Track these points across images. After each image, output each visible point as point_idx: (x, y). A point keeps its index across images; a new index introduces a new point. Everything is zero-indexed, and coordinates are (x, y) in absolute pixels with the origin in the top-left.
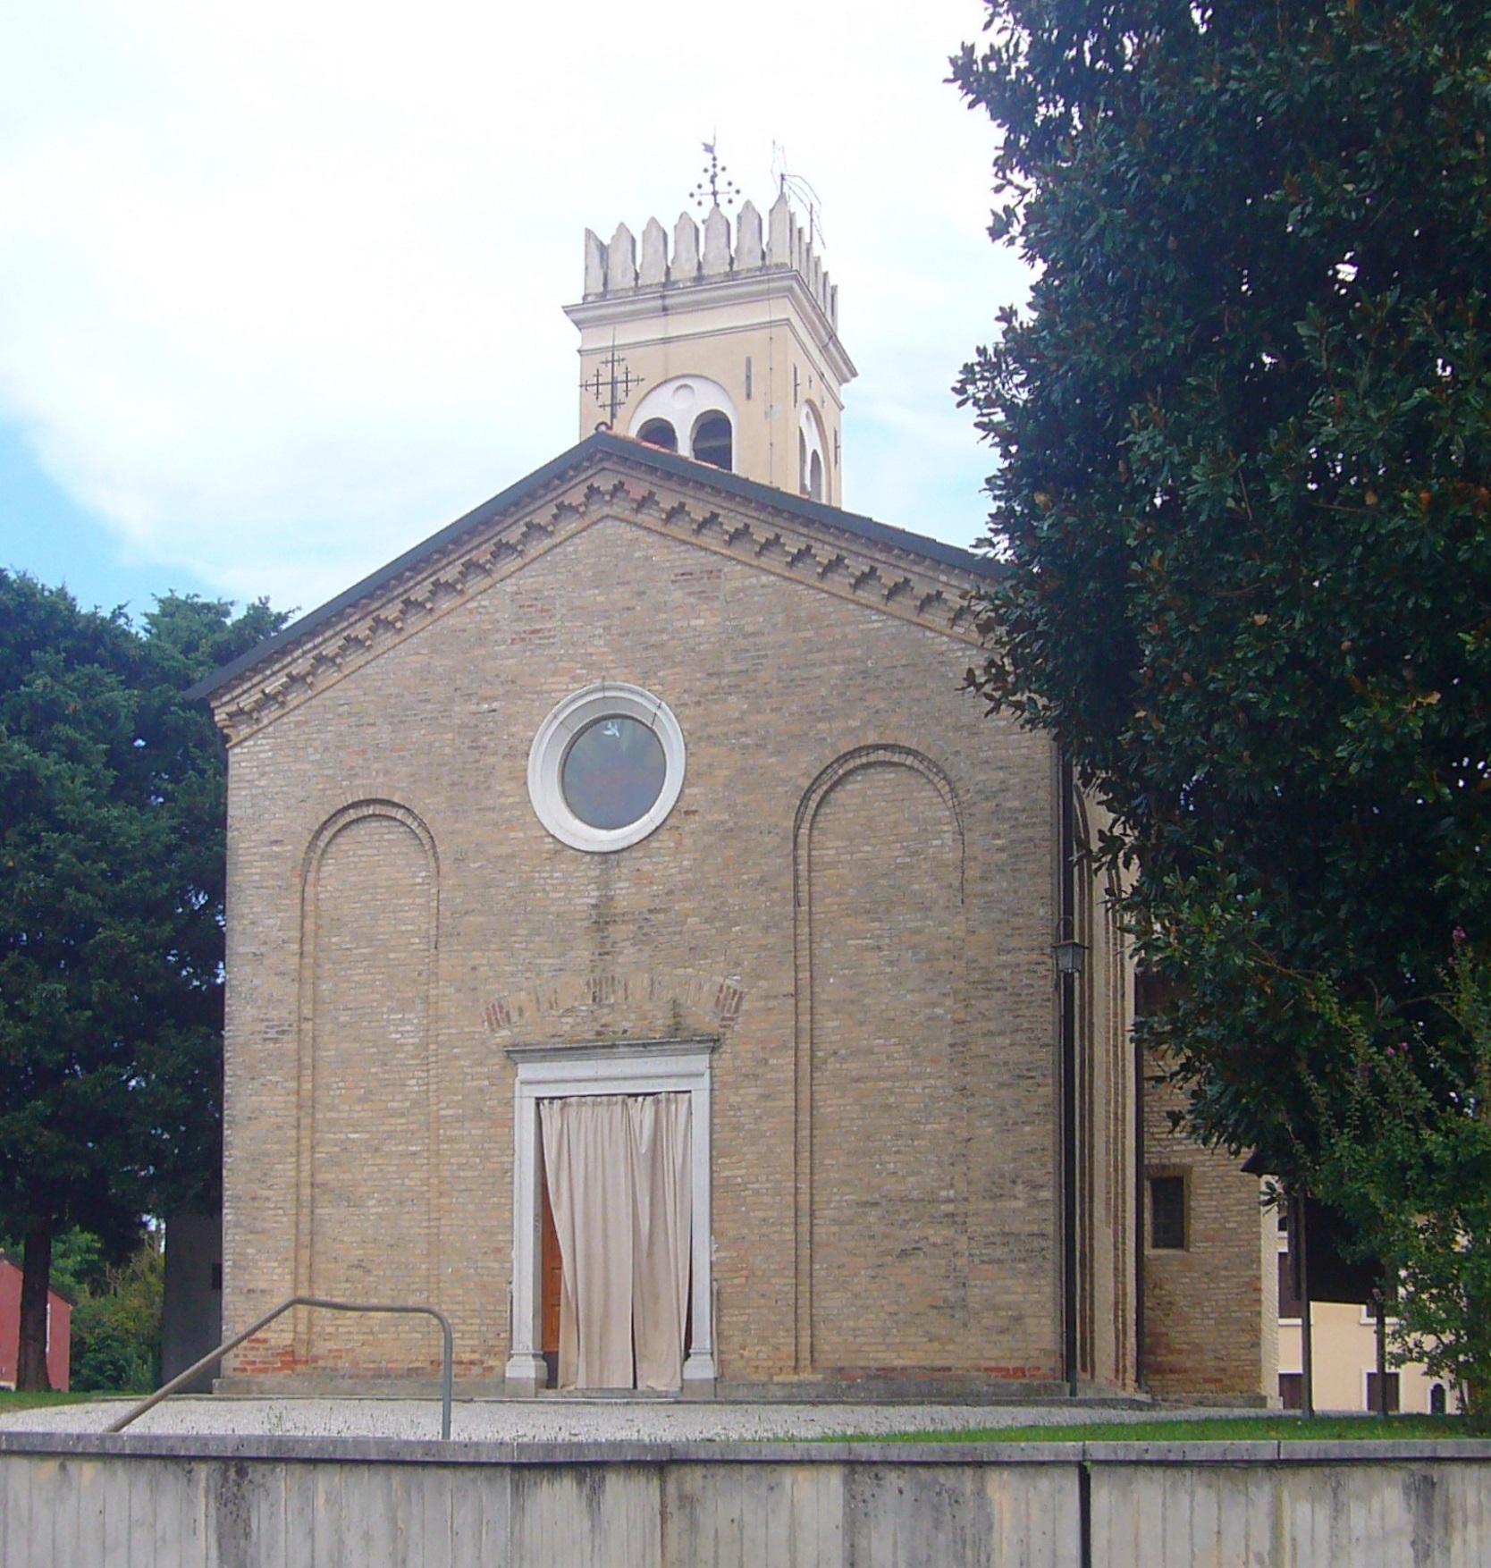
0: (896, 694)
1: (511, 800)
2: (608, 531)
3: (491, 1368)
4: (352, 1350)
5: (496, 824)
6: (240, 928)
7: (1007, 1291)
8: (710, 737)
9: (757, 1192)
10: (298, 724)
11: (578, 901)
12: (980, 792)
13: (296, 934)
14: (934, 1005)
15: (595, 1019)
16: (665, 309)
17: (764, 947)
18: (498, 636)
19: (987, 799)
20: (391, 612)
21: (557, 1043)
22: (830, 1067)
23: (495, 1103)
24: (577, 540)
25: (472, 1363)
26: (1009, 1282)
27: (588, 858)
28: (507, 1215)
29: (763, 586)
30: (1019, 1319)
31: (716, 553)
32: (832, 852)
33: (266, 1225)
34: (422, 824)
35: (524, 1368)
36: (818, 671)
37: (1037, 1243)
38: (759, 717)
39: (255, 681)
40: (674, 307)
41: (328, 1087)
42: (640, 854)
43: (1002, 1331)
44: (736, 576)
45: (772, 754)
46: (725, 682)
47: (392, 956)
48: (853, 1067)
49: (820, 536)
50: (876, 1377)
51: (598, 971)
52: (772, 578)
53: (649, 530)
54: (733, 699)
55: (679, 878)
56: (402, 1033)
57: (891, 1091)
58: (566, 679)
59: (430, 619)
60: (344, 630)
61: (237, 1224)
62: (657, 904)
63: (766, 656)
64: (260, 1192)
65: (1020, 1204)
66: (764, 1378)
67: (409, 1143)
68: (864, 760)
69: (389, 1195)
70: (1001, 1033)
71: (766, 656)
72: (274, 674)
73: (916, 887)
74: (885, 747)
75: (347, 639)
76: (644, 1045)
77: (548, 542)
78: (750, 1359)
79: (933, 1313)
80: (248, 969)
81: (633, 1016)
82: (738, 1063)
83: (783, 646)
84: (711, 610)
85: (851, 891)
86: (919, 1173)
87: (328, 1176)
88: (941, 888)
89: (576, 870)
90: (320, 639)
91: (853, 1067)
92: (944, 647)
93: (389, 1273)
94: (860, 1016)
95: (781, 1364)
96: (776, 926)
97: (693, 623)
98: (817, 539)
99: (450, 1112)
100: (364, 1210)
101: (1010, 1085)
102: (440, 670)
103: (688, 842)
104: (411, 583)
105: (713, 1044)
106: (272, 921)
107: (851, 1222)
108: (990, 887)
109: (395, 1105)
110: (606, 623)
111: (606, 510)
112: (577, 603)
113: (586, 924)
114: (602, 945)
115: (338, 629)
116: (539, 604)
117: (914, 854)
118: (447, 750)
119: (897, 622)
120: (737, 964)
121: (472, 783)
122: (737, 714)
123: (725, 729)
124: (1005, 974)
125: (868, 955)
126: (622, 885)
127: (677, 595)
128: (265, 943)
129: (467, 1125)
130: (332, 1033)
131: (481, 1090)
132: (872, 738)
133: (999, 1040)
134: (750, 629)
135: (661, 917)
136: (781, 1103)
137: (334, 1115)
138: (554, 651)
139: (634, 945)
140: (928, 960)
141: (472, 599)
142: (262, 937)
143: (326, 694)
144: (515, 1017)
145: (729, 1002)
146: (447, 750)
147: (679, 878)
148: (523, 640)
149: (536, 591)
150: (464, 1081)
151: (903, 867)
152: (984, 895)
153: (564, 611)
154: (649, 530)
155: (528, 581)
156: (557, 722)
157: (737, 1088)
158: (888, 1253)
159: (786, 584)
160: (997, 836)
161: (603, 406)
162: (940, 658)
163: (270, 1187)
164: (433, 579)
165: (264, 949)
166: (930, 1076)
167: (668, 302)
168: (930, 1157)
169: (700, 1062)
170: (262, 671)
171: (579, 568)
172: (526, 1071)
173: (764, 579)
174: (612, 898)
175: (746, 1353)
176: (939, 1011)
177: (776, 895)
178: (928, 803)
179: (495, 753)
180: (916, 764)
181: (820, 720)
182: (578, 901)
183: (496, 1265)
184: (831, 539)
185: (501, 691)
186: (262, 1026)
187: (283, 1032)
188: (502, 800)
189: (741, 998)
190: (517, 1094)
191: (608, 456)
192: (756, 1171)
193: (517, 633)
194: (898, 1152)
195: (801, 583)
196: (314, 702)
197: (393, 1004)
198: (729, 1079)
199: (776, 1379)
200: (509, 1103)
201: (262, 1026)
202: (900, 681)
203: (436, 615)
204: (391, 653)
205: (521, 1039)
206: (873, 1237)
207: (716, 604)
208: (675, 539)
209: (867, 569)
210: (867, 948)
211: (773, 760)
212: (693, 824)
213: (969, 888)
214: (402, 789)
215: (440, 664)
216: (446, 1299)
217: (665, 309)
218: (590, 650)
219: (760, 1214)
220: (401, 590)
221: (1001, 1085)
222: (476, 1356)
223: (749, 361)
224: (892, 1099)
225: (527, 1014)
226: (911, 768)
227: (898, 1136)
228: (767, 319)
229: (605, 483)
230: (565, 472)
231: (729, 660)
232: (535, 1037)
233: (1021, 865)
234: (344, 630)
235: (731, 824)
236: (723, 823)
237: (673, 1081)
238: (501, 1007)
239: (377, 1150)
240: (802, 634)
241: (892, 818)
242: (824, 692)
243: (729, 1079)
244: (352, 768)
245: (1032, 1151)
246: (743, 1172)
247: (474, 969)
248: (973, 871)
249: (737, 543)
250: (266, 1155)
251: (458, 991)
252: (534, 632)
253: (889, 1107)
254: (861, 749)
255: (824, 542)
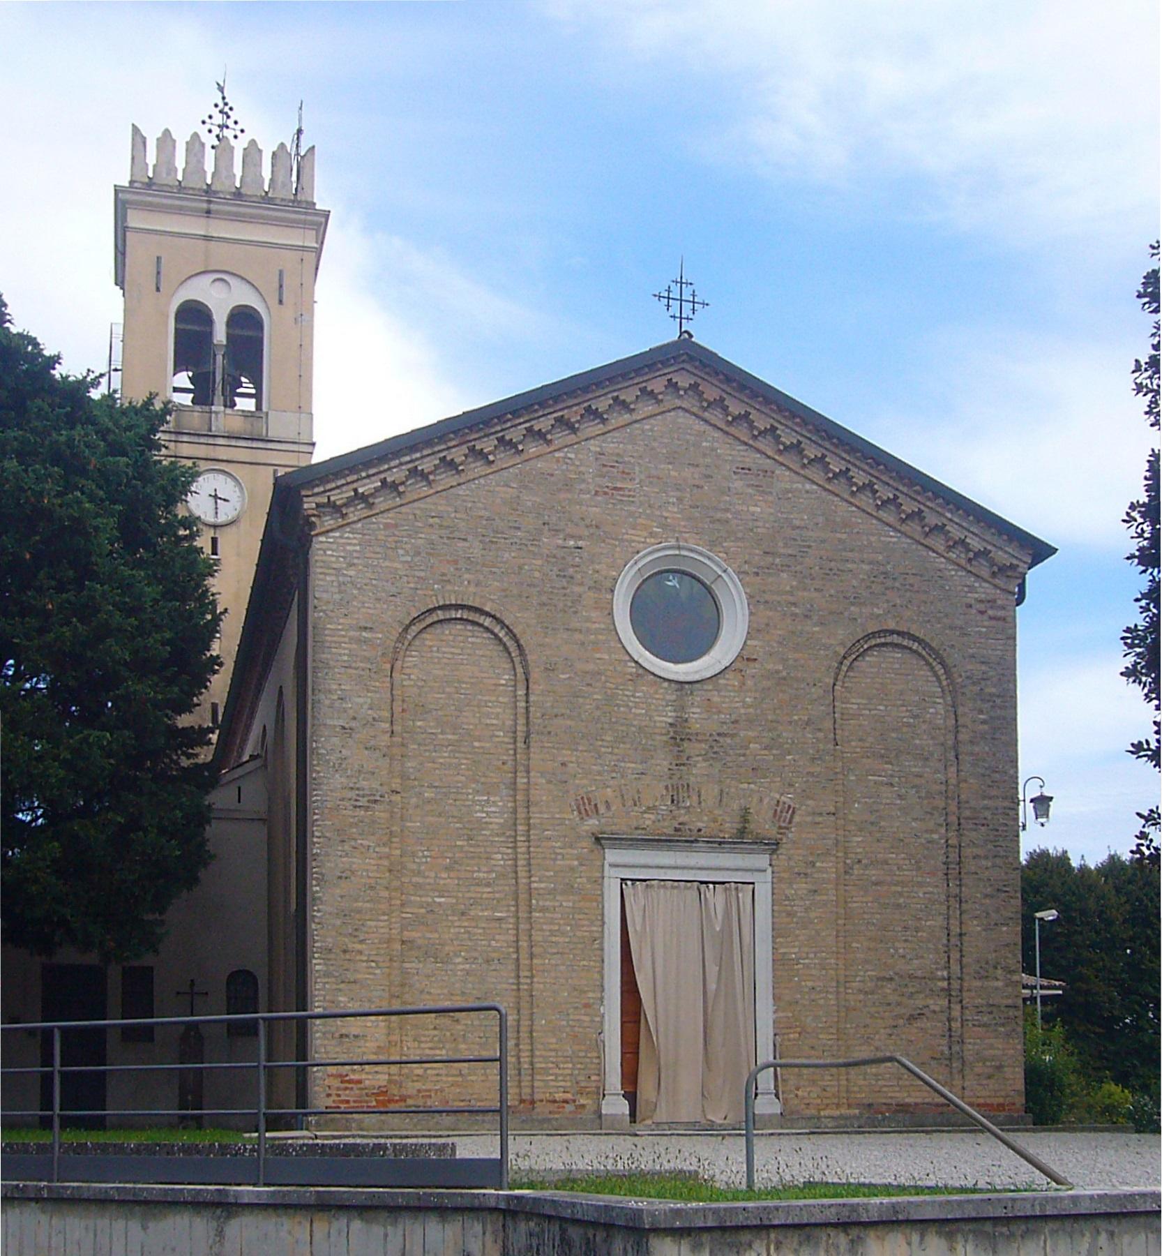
0: (908, 594)
1: (597, 626)
2: (680, 420)
3: (583, 1106)
4: (442, 1090)
5: (583, 644)
6: (327, 702)
7: (991, 1047)
8: (766, 602)
9: (807, 966)
10: (387, 526)
11: (657, 718)
12: (968, 677)
13: (387, 714)
14: (932, 832)
15: (674, 818)
16: (208, 212)
17: (812, 774)
18: (583, 486)
19: (974, 684)
20: (488, 445)
21: (638, 834)
22: (856, 872)
23: (585, 880)
24: (652, 421)
25: (566, 1101)
26: (992, 1041)
27: (666, 684)
28: (597, 976)
29: (807, 492)
30: (999, 1068)
31: (769, 457)
32: (855, 707)
33: (359, 976)
34: (510, 631)
35: (616, 1106)
36: (850, 566)
37: (1011, 1013)
38: (805, 594)
39: (349, 479)
40: (217, 212)
41: (414, 855)
42: (710, 687)
43: (989, 1077)
44: (784, 479)
45: (815, 625)
46: (778, 561)
47: (476, 744)
48: (874, 874)
49: (858, 463)
50: (897, 1111)
51: (675, 778)
52: (815, 487)
53: (715, 426)
54: (784, 575)
55: (742, 711)
56: (487, 813)
57: (901, 894)
58: (645, 534)
59: (518, 459)
60: (440, 451)
61: (327, 974)
62: (724, 729)
63: (809, 547)
64: (350, 946)
65: (1000, 984)
66: (814, 1112)
67: (494, 910)
68: (883, 640)
69: (475, 954)
70: (986, 858)
71: (809, 547)
72: (368, 476)
73: (917, 742)
74: (899, 633)
75: (443, 459)
76: (720, 843)
77: (627, 417)
78: (804, 1098)
79: (933, 1063)
80: (335, 740)
81: (705, 818)
82: (792, 863)
83: (823, 541)
84: (766, 502)
85: (870, 739)
86: (922, 957)
87: (414, 934)
88: (935, 745)
89: (656, 693)
90: (418, 455)
91: (874, 874)
92: (942, 566)
93: (476, 1022)
94: (878, 835)
95: (826, 1101)
96: (820, 759)
97: (752, 509)
98: (855, 465)
99: (543, 885)
100: (451, 967)
101: (991, 896)
102: (529, 504)
103: (749, 683)
104: (509, 424)
105: (773, 846)
106: (360, 700)
107: (872, 993)
108: (977, 749)
109: (481, 875)
110: (678, 494)
111: (678, 403)
112: (654, 472)
113: (665, 738)
114: (678, 757)
115: (436, 449)
116: (621, 466)
117: (915, 717)
118: (537, 574)
119: (909, 541)
120: (791, 785)
121: (561, 605)
122: (788, 588)
123: (779, 599)
124: (987, 814)
125: (883, 789)
126: (694, 710)
127: (738, 484)
128: (354, 718)
129: (558, 898)
130: (417, 806)
131: (572, 869)
132: (892, 625)
133: (984, 862)
134: (797, 523)
135: (729, 740)
136: (825, 898)
137: (420, 880)
138: (632, 508)
139: (705, 760)
140: (927, 798)
141: (559, 450)
142: (351, 712)
143: (416, 505)
144: (602, 809)
145: (784, 814)
146: (537, 574)
147: (742, 711)
148: (606, 493)
149: (618, 455)
150: (555, 859)
151: (909, 725)
152: (972, 754)
153: (643, 477)
154: (715, 426)
155: (611, 445)
156: (636, 568)
157: (791, 884)
158: (900, 1016)
159: (824, 494)
160: (981, 712)
161: (674, 317)
162: (939, 573)
163: (361, 942)
164: (527, 425)
165: (353, 724)
166: (929, 884)
167: (213, 207)
168: (930, 945)
169: (762, 860)
170: (358, 472)
171: (655, 444)
172: (612, 856)
173: (808, 486)
174: (686, 720)
175: (800, 1093)
176: (935, 836)
177: (821, 735)
178: (923, 678)
179: (582, 584)
180: (920, 650)
181: (853, 604)
182: (657, 718)
183: (587, 1018)
184: (866, 468)
185: (587, 533)
186: (352, 794)
187: (376, 801)
188: (588, 625)
189: (794, 812)
190: (606, 874)
191: (691, 359)
192: (806, 949)
193: (600, 486)
194: (906, 941)
195: (837, 495)
196: (403, 509)
197: (479, 787)
198: (785, 875)
199: (822, 1113)
200: (599, 881)
201: (352, 794)
202: (912, 585)
203: (525, 456)
204: (482, 481)
205: (608, 829)
206: (889, 1004)
207: (770, 498)
208: (738, 439)
209: (891, 496)
210: (882, 783)
211: (816, 629)
212: (752, 670)
213: (962, 749)
214: (493, 600)
215: (529, 499)
216: (539, 1046)
217: (208, 212)
218: (665, 514)
219: (810, 984)
220: (499, 428)
221: (986, 896)
222: (569, 1096)
223: (281, 273)
224: (901, 900)
225: (613, 808)
226: (915, 652)
227: (906, 928)
228: (202, 233)
229: (683, 381)
230: (654, 364)
231: (781, 544)
232: (621, 826)
233: (997, 736)
234: (440, 451)
235: (784, 674)
236: (777, 672)
237: (740, 873)
238: (589, 799)
239: (463, 914)
240: (838, 535)
241: (901, 687)
242: (855, 583)
243: (785, 875)
244: (443, 575)
245: (1007, 945)
246: (796, 950)
247: (563, 764)
248: (964, 736)
249: (786, 454)
250: (359, 911)
251: (549, 782)
252: (615, 489)
253: (899, 905)
254: (879, 632)
255: (859, 468)
